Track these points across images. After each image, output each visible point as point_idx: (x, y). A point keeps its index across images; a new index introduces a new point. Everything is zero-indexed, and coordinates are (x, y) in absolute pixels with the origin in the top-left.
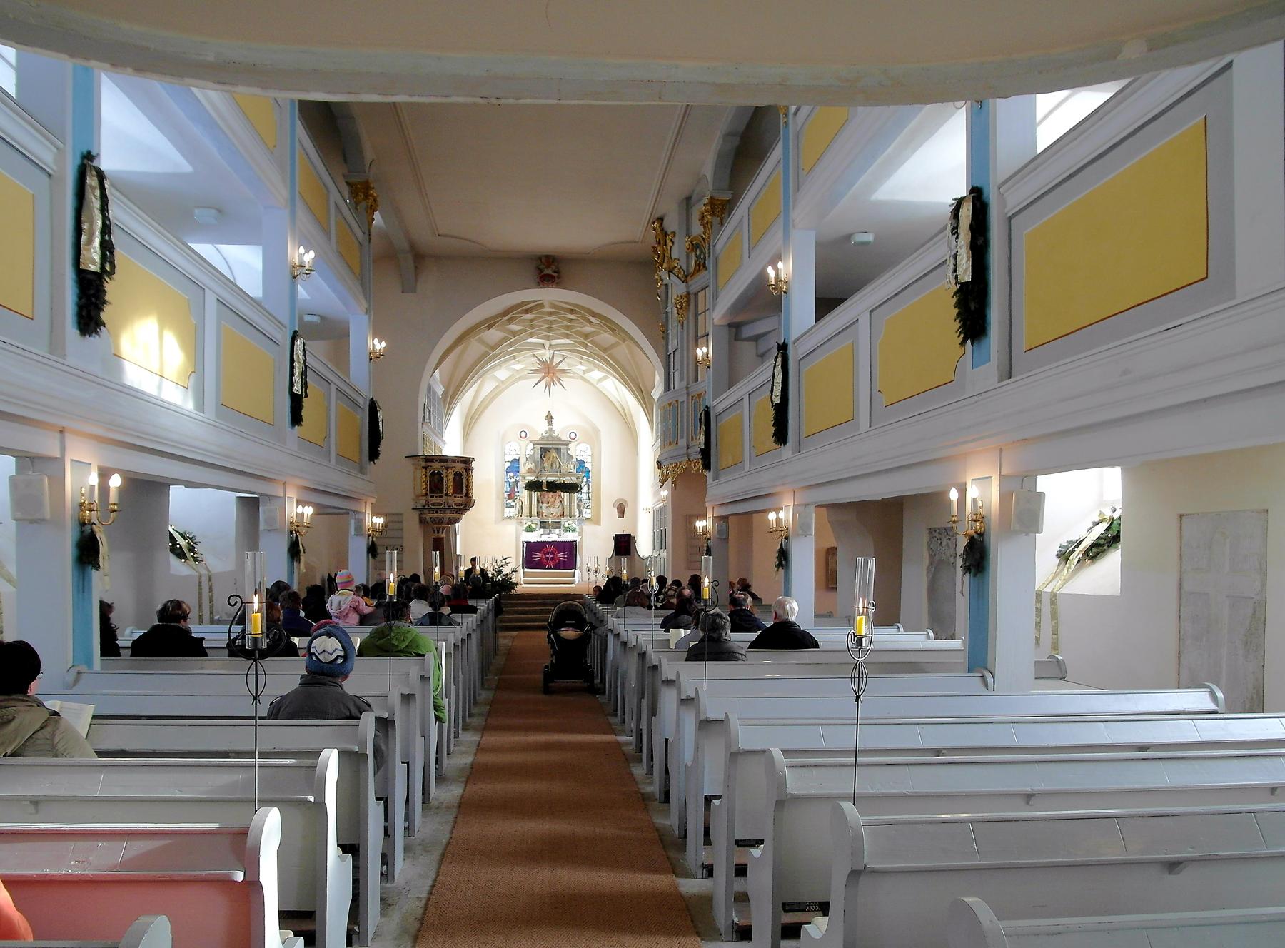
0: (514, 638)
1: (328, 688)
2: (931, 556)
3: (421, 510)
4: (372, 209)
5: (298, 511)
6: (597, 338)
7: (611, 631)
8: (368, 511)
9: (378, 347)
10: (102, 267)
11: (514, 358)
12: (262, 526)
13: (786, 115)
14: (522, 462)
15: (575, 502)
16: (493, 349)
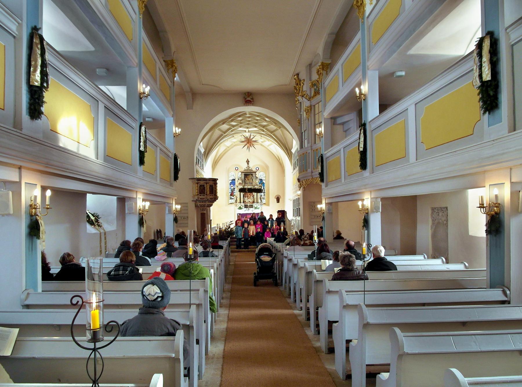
0: (236, 256)
1: (155, 316)
2: (433, 220)
3: (196, 201)
4: (175, 72)
5: (141, 203)
6: (268, 127)
7: (286, 257)
8: (174, 203)
9: (177, 131)
10: (42, 83)
11: (233, 136)
12: (127, 211)
13: (363, 19)
14: (236, 180)
15: (259, 197)
16: (225, 133)
